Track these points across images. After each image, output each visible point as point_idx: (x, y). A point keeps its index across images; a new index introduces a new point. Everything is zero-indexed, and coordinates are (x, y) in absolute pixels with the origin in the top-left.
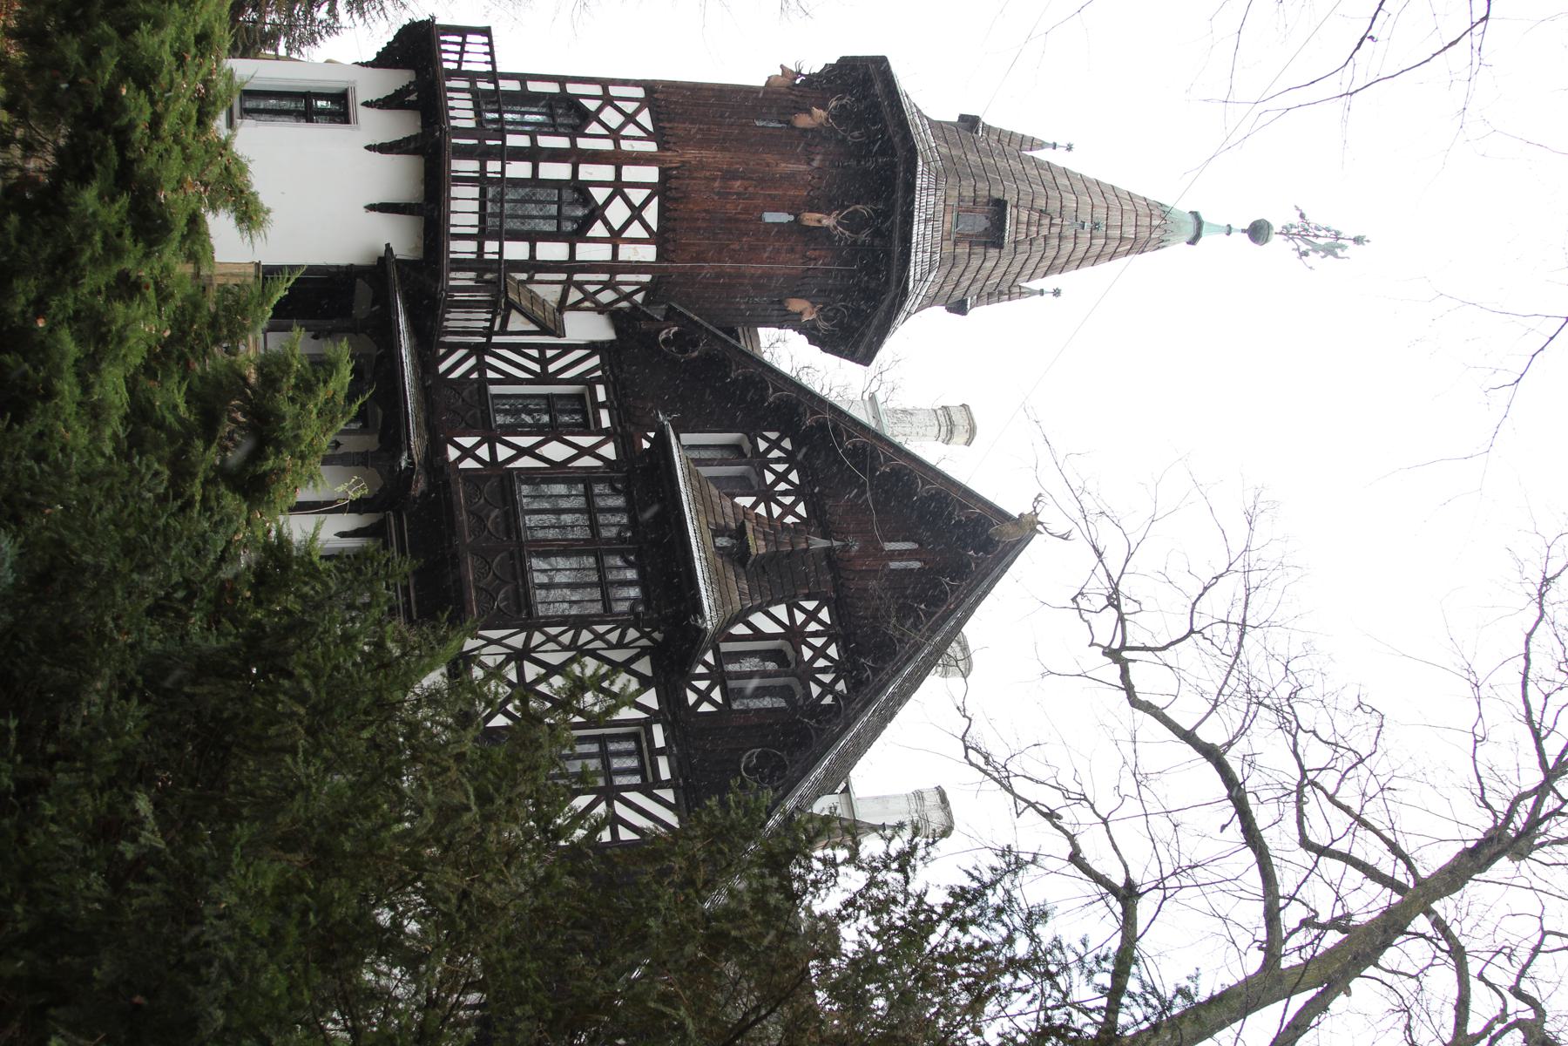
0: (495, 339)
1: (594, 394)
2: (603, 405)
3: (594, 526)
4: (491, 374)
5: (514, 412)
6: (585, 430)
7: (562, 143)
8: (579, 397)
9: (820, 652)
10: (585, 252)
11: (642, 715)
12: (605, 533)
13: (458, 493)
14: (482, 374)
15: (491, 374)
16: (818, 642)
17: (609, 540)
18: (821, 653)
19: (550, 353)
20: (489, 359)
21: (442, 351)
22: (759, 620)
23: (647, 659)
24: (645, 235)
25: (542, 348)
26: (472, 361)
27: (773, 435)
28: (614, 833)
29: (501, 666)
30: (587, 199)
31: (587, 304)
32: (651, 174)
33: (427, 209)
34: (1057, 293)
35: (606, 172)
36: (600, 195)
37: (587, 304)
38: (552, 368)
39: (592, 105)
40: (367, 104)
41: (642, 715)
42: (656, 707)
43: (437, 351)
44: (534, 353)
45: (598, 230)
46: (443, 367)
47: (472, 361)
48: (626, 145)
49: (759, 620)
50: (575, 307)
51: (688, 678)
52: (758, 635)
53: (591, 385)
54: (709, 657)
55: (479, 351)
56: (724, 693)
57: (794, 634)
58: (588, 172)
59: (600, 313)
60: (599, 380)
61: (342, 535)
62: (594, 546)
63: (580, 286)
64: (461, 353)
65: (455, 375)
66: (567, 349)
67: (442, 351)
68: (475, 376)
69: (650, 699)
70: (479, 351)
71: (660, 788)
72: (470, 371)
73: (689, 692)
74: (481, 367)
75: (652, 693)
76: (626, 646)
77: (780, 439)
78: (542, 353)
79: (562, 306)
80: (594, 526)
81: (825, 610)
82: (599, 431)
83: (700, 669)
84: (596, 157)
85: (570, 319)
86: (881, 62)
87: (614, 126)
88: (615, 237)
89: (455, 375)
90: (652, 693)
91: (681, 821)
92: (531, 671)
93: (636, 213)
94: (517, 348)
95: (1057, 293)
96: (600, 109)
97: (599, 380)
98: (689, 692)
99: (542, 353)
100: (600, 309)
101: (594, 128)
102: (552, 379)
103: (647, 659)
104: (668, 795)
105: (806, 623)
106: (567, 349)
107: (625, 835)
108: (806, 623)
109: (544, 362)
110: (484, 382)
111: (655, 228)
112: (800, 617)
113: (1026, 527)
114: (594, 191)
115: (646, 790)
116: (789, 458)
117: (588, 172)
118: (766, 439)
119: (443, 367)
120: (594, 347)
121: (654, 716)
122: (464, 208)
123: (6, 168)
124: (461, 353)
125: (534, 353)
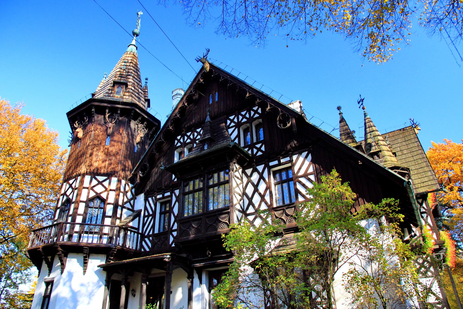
0: (140, 232)
1: (160, 199)
3: (199, 190)
4: (151, 233)
6: (170, 202)
7: (73, 206)
8: (162, 204)
9: (244, 117)
11: (266, 170)
12: (201, 186)
13: (184, 239)
14: (151, 236)
15: (151, 233)
17: (204, 185)
20: (146, 234)
21: (143, 250)
23: (247, 171)
24: (108, 181)
26: (146, 239)
27: (176, 142)
28: (311, 174)
29: (249, 221)
30: (92, 200)
31: (132, 202)
34: (147, 79)
36: (92, 194)
37: (132, 202)
38: (151, 213)
39: (65, 198)
41: (266, 170)
42: (263, 165)
43: (143, 252)
44: (146, 219)
45: (104, 196)
46: (148, 250)
47: (146, 239)
49: (233, 137)
51: (254, 156)
52: (238, 136)
53: (157, 200)
54: (246, 149)
55: (143, 236)
56: (257, 143)
57: (238, 125)
58: (84, 197)
59: (136, 198)
60: (156, 197)
61: (201, 283)
62: (206, 189)
63: (124, 203)
67: (143, 250)
68: (151, 238)
69: (260, 168)
70: (143, 236)
71: (293, 160)
73: (258, 155)
74: (148, 236)
76: (242, 178)
77: (177, 140)
79: (132, 210)
80: (199, 190)
82: (171, 196)
83: (250, 152)
85: (136, 208)
86: (68, 114)
91: (305, 151)
92: (251, 210)
93: (100, 183)
94: (144, 225)
95: (147, 79)
98: (258, 155)
100: (134, 198)
101: (71, 197)
102: (154, 212)
103: (247, 171)
104: (295, 157)
105: (234, 122)
106: (146, 208)
107: (311, 170)
108: (234, 122)
109: (149, 215)
110: (154, 235)
112: (233, 124)
114: (90, 197)
115: (293, 165)
116: (183, 136)
118: (177, 144)
119: (148, 250)
120: (146, 200)
121: (267, 166)
122: (87, 240)
123: (460, 190)
125: (146, 219)
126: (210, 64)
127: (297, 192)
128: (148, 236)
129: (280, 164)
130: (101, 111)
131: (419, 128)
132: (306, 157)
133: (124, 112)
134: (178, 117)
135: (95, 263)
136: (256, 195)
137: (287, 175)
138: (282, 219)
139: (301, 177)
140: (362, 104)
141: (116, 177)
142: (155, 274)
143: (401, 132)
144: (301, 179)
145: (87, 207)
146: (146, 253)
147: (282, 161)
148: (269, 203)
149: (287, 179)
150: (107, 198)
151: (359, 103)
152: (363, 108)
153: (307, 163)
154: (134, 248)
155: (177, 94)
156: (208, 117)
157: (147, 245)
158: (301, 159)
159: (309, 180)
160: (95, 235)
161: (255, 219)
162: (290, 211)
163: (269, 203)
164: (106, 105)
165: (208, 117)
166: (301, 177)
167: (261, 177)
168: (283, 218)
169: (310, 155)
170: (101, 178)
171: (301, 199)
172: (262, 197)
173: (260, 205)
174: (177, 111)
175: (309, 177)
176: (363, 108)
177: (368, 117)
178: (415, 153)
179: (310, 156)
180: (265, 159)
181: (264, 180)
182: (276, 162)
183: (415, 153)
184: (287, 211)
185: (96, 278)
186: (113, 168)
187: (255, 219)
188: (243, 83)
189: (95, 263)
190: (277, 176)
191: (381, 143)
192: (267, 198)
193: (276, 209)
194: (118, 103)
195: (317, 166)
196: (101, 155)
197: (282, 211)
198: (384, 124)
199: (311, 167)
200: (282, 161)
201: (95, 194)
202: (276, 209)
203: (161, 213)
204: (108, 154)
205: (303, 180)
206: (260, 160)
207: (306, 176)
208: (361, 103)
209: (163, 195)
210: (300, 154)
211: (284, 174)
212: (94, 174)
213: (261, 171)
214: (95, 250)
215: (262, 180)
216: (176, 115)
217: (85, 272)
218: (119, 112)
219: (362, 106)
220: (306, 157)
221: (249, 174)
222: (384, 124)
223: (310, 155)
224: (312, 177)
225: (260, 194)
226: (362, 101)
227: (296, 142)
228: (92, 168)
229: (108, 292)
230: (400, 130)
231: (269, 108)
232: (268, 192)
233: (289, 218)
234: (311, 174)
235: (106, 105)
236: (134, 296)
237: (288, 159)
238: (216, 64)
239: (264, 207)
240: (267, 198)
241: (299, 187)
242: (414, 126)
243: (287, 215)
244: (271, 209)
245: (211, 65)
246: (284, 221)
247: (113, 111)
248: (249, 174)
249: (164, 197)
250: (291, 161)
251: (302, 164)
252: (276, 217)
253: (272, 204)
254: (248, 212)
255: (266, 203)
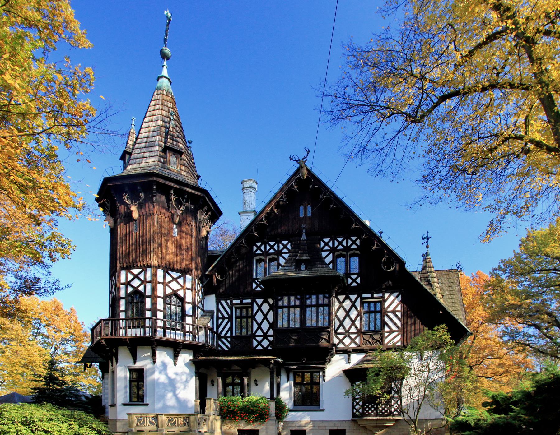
2: (242, 301)
4: (229, 334)
5: (241, 328)
7: (148, 302)
9: (340, 243)
10: (149, 293)
14: (229, 337)
15: (229, 334)
16: (350, 242)
18: (341, 242)
19: (220, 316)
22: (328, 260)
25: (218, 318)
28: (398, 311)
30: (169, 296)
32: (123, 274)
33: (176, 348)
35: (160, 288)
36: (130, 289)
40: (135, 363)
44: (220, 321)
45: (141, 288)
48: (148, 279)
50: (203, 306)
52: (332, 262)
55: (219, 337)
57: (333, 250)
58: (123, 293)
61: (288, 380)
62: (303, 308)
64: (220, 342)
65: (229, 345)
66: (218, 310)
67: (219, 349)
69: (353, 297)
72: (228, 341)
74: (225, 337)
75: (351, 296)
78: (220, 318)
81: (352, 238)
82: (252, 304)
84: (154, 289)
87: (132, 283)
88: (143, 282)
89: (229, 345)
90: (351, 296)
94: (218, 326)
96: (132, 286)
97: (231, 302)
99: (220, 318)
104: (387, 295)
106: (218, 310)
107: (399, 308)
109: (223, 318)
111: (180, 274)
113: (302, 164)
114: (129, 292)
115: (385, 301)
117: (123, 293)
120: (218, 302)
121: (360, 296)
122: (178, 336)
124: (220, 342)
125: (220, 321)
126: (307, 169)
127: (385, 323)
128: (225, 337)
129: (372, 297)
130: (165, 190)
131: (462, 273)
132: (397, 297)
133: (192, 198)
134: (264, 224)
135: (185, 357)
136: (347, 320)
137: (375, 307)
138: (369, 341)
139: (390, 312)
140: (427, 242)
141: (190, 275)
142: (235, 370)
143: (447, 273)
144: (389, 314)
145: (165, 303)
146: (224, 353)
147: (375, 295)
148: (359, 328)
149: (377, 311)
150: (185, 295)
151: (424, 239)
152: (427, 247)
153: (396, 302)
154: (142, 334)
155: (250, 187)
156: (304, 234)
157: (225, 345)
158: (392, 298)
159: (396, 316)
160: (177, 332)
161: (345, 337)
162: (377, 337)
163: (359, 328)
164: (172, 184)
165: (304, 234)
166: (390, 312)
167: (353, 305)
168: (370, 340)
169: (400, 296)
170: (175, 275)
171: (387, 329)
172: (353, 322)
173: (350, 327)
174: (264, 215)
175: (397, 313)
176: (427, 247)
177: (429, 256)
178: (455, 296)
179: (400, 297)
180: (359, 291)
181: (356, 308)
182: (369, 295)
183: (455, 296)
184: (374, 336)
185: (187, 370)
186: (186, 265)
187: (345, 337)
188: (351, 213)
189: (185, 357)
190: (366, 305)
191: (436, 285)
192: (357, 323)
193: (364, 333)
194: (187, 185)
195: (405, 306)
196: (172, 247)
197: (369, 336)
198: (439, 263)
199: (399, 306)
200: (375, 295)
201: (171, 291)
202: (364, 333)
203: (236, 317)
204: (179, 247)
205: (391, 315)
206: (353, 291)
207: (394, 312)
208: (426, 240)
209: (242, 301)
210: (392, 293)
211: (372, 305)
212: (168, 269)
213: (353, 300)
214: (187, 347)
215: (353, 308)
216: (262, 220)
217: (175, 364)
218: (186, 196)
219: (426, 244)
220: (397, 297)
221: (341, 300)
222: (439, 263)
223: (400, 296)
224: (399, 314)
225: (351, 319)
226: (428, 239)
227: (390, 282)
228: (164, 262)
229: (198, 380)
230: (446, 270)
231: (375, 247)
232: (359, 318)
233: (375, 341)
234: (398, 311)
235: (172, 184)
236: (213, 385)
237: (381, 295)
238: (316, 172)
239: (353, 330)
240: (357, 323)
241: (386, 319)
242: (458, 270)
243: (373, 339)
244: (360, 332)
245: (309, 172)
246: (370, 343)
247: (180, 193)
248: (341, 300)
249: (242, 303)
250: (383, 297)
251: (393, 302)
252: (364, 339)
253: (361, 328)
254: (339, 331)
255: (356, 327)
